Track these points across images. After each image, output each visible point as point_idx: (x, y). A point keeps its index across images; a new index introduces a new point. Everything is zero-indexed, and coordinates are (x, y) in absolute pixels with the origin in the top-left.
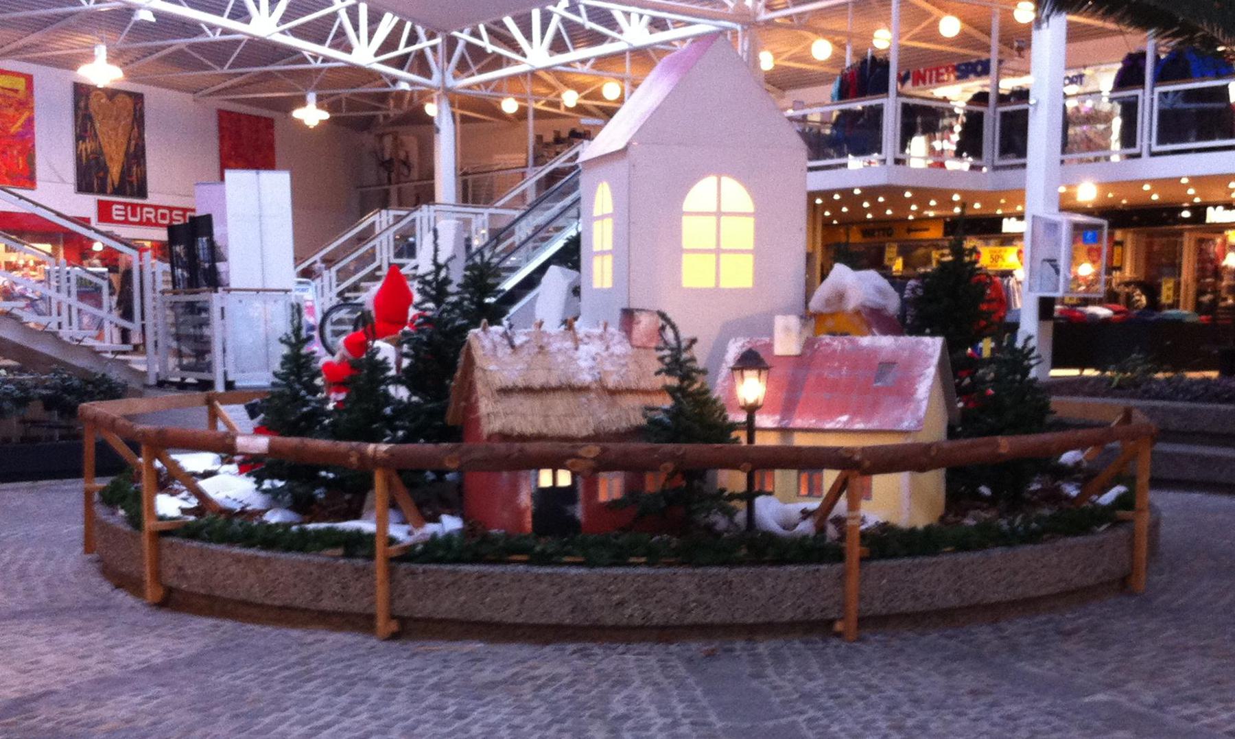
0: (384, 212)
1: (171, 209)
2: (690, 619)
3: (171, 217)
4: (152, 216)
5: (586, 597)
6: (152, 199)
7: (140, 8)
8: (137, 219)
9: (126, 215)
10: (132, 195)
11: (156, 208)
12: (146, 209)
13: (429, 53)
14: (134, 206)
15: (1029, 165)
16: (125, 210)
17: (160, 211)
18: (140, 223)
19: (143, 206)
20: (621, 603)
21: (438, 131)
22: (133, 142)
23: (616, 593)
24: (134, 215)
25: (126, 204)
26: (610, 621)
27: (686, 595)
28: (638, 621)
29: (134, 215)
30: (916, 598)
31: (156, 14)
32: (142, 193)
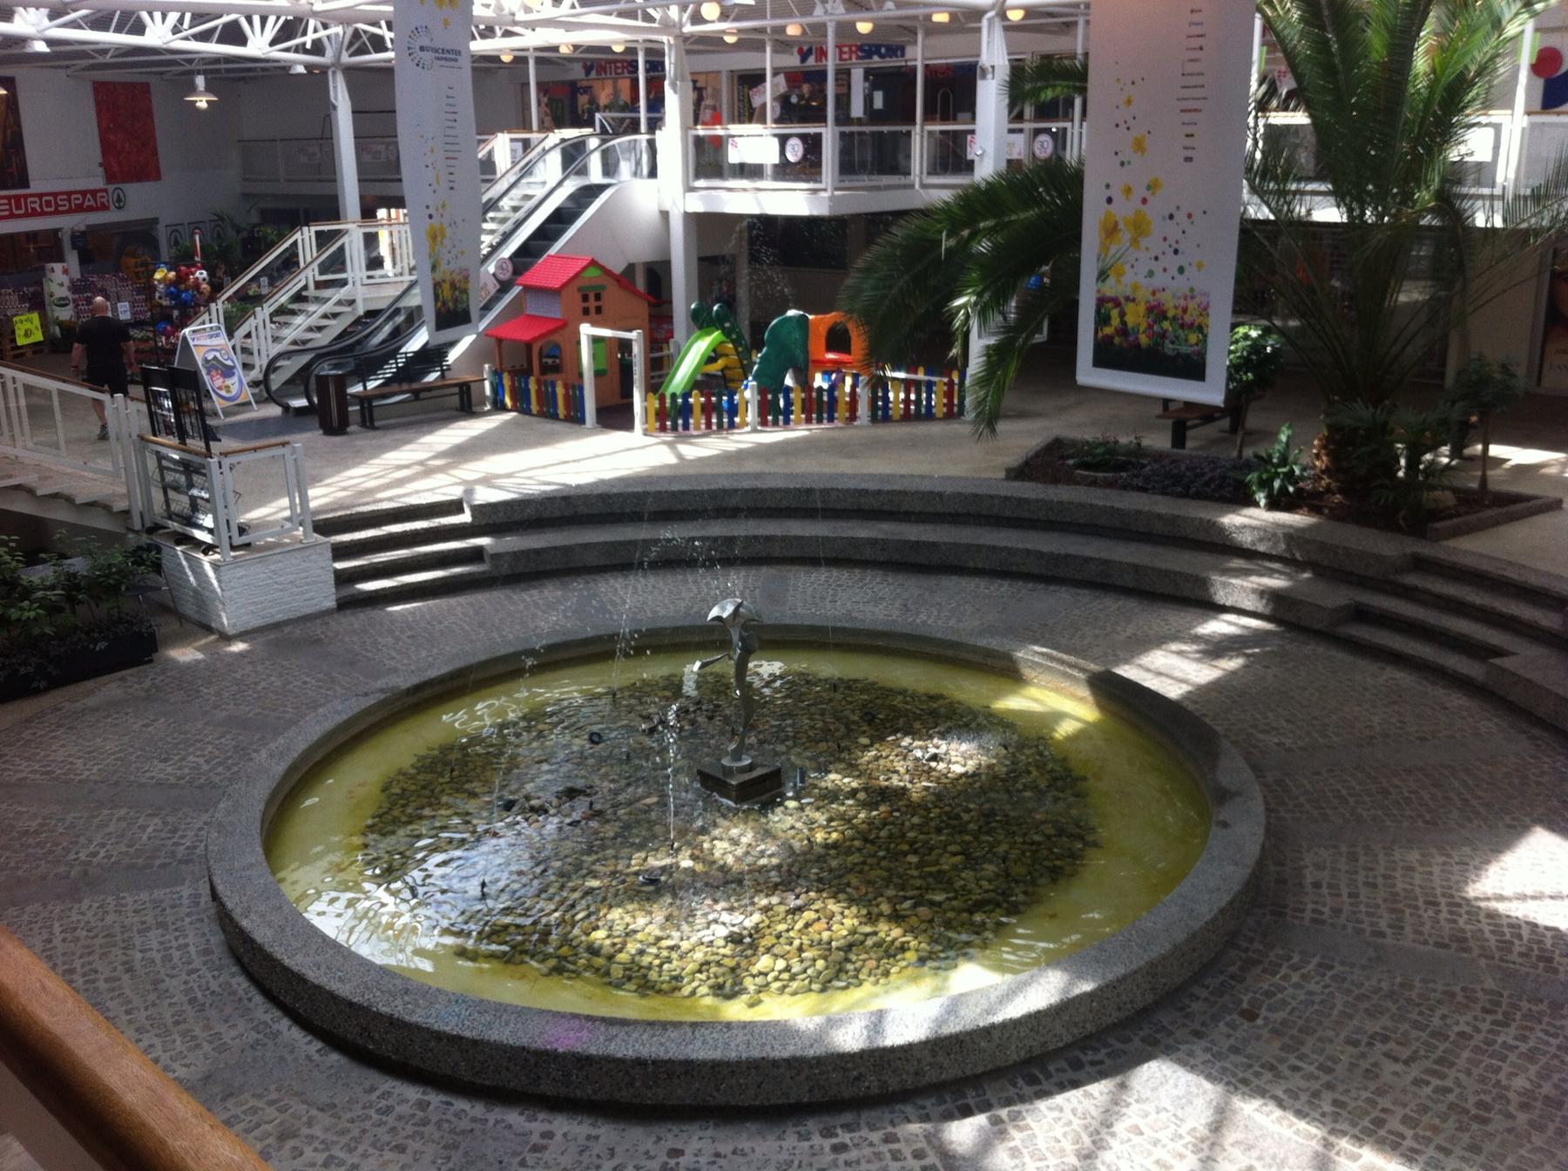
0: (305, 229)
1: (55, 195)
2: (925, 1081)
3: (56, 203)
4: (37, 206)
5: (824, 1077)
6: (36, 186)
7: (33, 39)
8: (22, 212)
9: (11, 210)
10: (14, 187)
11: (40, 196)
12: (29, 200)
13: (325, 41)
14: (17, 198)
15: (977, 132)
16: (10, 204)
17: (44, 199)
18: (26, 215)
19: (26, 197)
20: (858, 1078)
21: (335, 108)
22: (9, 131)
23: (854, 1069)
24: (18, 207)
25: (9, 198)
26: (847, 1095)
27: (919, 1061)
28: (875, 1091)
29: (18, 207)
30: (1119, 1009)
31: (50, 42)
32: (25, 183)
